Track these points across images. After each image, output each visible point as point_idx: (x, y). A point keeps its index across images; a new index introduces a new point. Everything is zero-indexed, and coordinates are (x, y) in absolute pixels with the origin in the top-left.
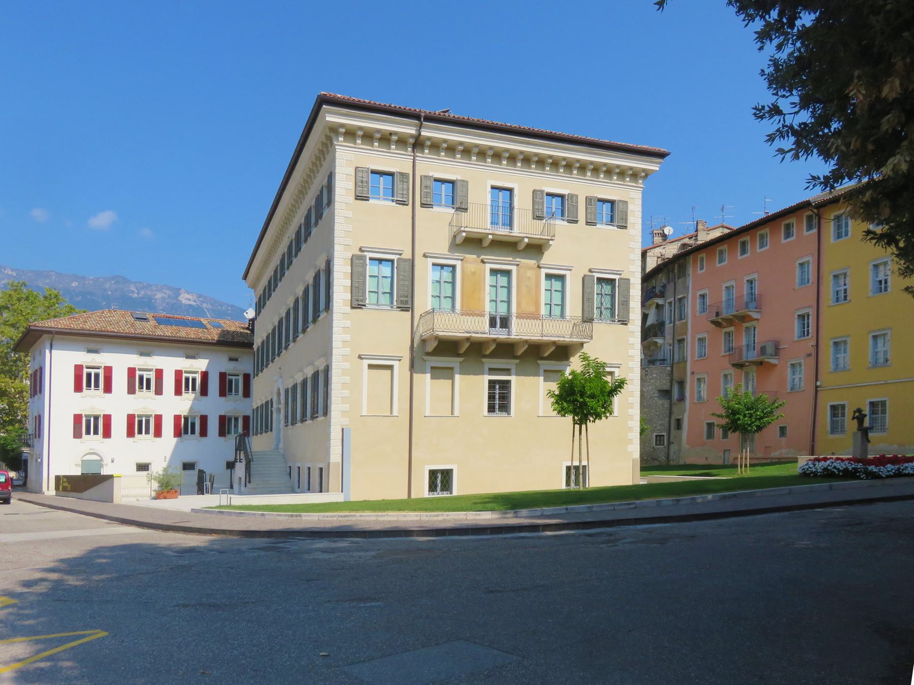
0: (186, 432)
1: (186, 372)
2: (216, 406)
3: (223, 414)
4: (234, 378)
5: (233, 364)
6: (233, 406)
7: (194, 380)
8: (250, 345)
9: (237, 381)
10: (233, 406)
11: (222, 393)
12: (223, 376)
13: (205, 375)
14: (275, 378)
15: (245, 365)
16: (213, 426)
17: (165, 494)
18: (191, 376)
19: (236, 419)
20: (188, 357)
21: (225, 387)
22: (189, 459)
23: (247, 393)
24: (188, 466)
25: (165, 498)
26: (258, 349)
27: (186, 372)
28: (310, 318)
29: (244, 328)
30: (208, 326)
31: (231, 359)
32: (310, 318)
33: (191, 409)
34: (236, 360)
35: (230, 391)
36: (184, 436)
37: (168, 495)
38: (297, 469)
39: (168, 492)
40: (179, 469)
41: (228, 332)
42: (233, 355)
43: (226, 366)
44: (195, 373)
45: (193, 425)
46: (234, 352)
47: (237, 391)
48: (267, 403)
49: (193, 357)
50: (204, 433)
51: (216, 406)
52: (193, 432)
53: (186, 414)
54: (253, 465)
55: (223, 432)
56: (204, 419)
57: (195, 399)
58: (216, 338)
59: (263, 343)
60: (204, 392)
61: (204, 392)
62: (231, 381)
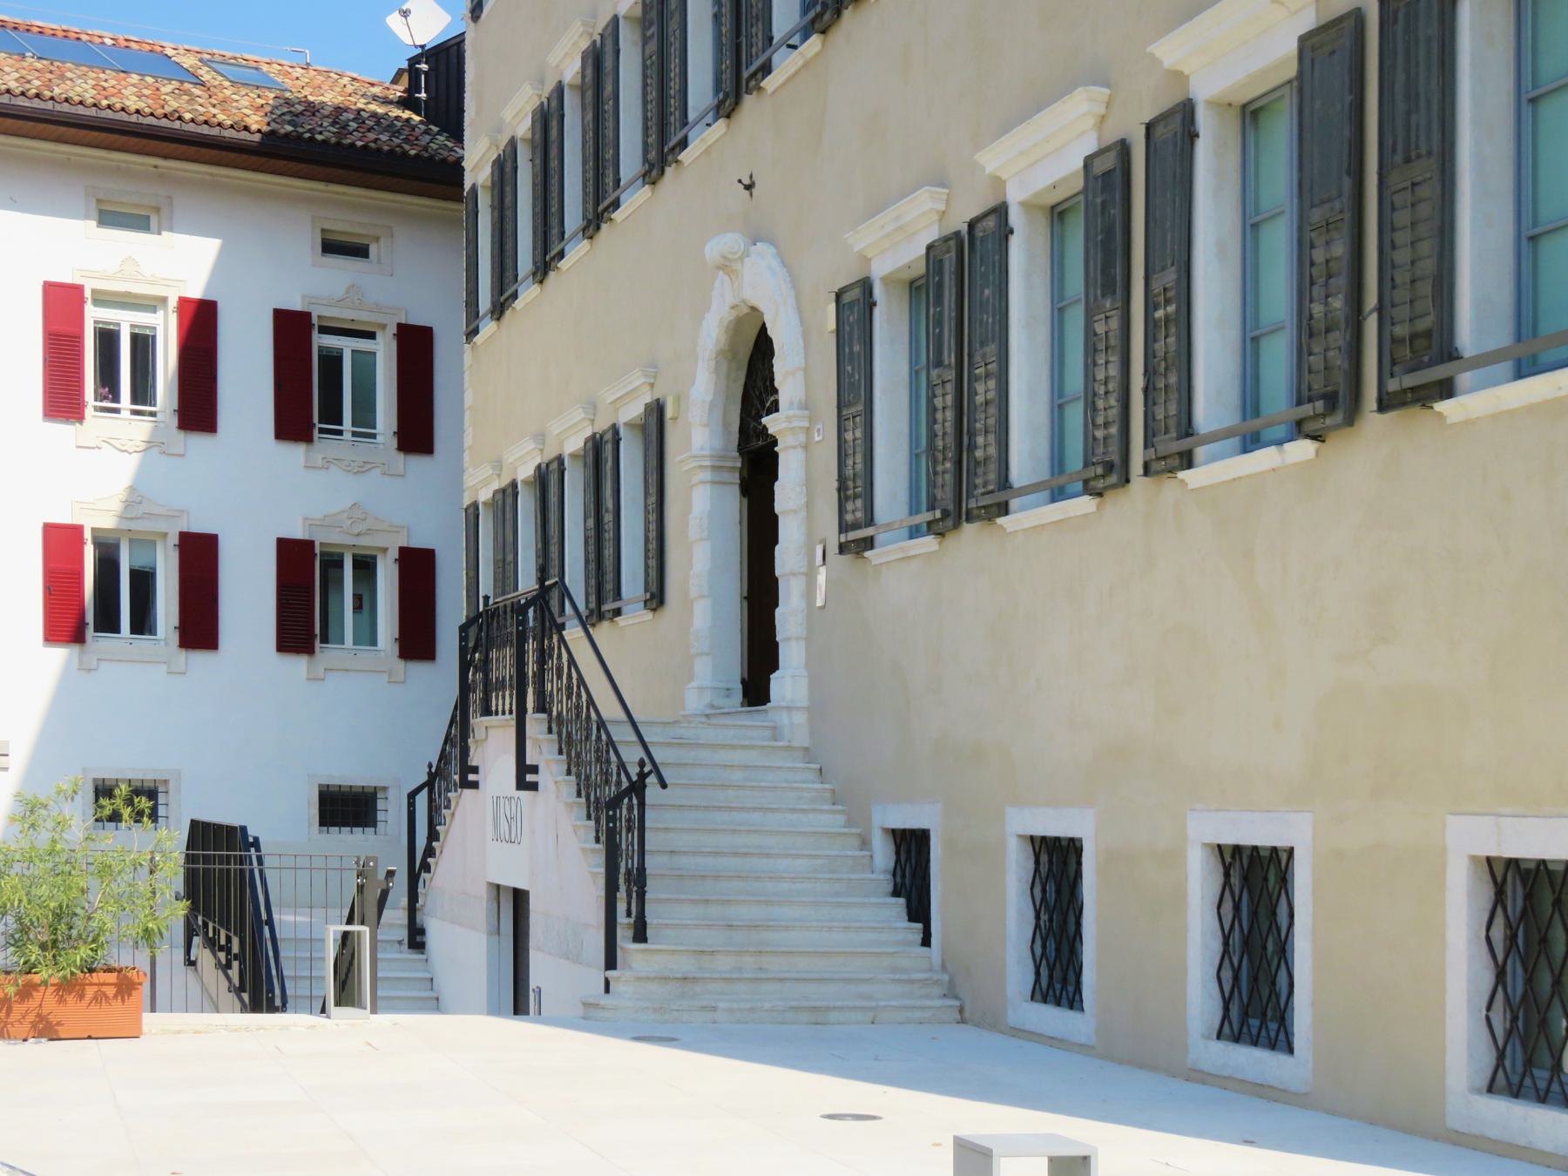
0: (107, 622)
1: (102, 299)
2: (259, 490)
3: (298, 533)
4: (347, 345)
5: (343, 270)
6: (344, 491)
7: (143, 345)
8: (439, 178)
9: (365, 364)
10: (344, 491)
11: (293, 423)
12: (291, 330)
13: (200, 323)
14: (715, 248)
15: (407, 276)
16: (248, 595)
17: (47, 1001)
18: (126, 322)
19: (365, 567)
20: (109, 217)
21: (308, 396)
22: (127, 765)
23: (416, 433)
24: (127, 800)
25: (47, 1030)
26: (504, 170)
27: (102, 299)
28: (573, 216)
29: (386, 101)
30: (206, 75)
31: (332, 247)
32: (573, 216)
33: (134, 500)
34: (358, 251)
35: (332, 414)
36: (100, 643)
37: (71, 1011)
38: (1016, 870)
39: (67, 987)
40: (78, 814)
41: (312, 109)
42: (346, 225)
43: (319, 286)
44: (152, 304)
45: (143, 582)
46: (350, 206)
47: (364, 414)
48: (600, 454)
49: (139, 223)
50: (199, 629)
51: (259, 490)
52: (143, 623)
53: (108, 522)
54: (668, 825)
55: (298, 629)
56: (199, 555)
57: (151, 444)
58: (256, 121)
59: (548, 120)
60: (198, 409)
61: (198, 409)
62: (332, 362)
